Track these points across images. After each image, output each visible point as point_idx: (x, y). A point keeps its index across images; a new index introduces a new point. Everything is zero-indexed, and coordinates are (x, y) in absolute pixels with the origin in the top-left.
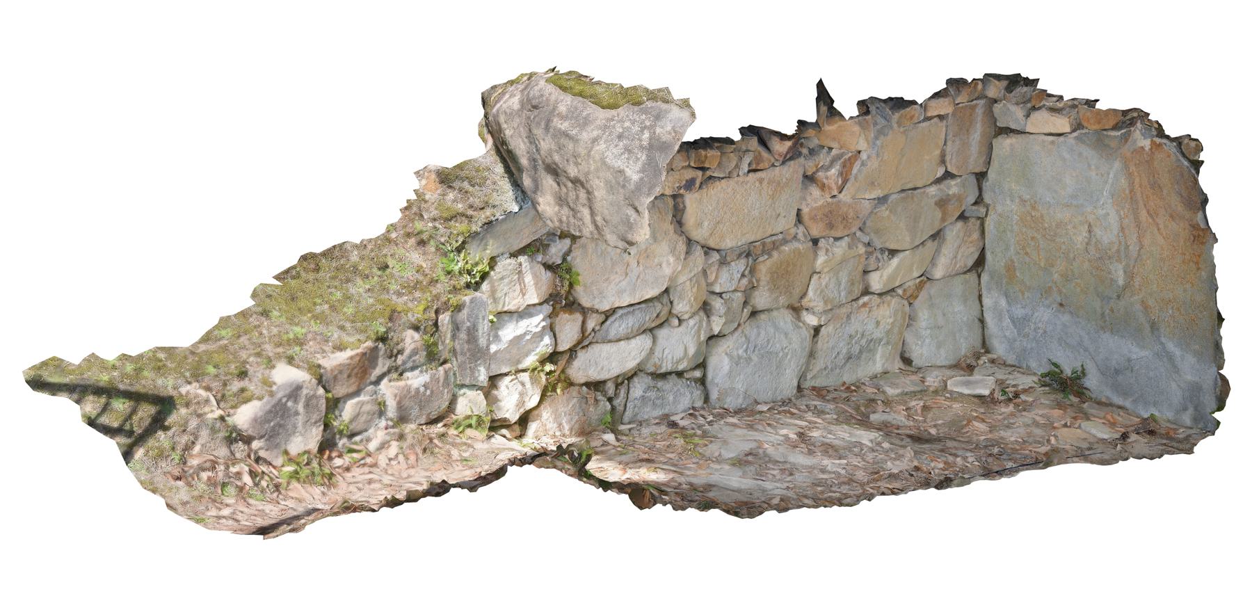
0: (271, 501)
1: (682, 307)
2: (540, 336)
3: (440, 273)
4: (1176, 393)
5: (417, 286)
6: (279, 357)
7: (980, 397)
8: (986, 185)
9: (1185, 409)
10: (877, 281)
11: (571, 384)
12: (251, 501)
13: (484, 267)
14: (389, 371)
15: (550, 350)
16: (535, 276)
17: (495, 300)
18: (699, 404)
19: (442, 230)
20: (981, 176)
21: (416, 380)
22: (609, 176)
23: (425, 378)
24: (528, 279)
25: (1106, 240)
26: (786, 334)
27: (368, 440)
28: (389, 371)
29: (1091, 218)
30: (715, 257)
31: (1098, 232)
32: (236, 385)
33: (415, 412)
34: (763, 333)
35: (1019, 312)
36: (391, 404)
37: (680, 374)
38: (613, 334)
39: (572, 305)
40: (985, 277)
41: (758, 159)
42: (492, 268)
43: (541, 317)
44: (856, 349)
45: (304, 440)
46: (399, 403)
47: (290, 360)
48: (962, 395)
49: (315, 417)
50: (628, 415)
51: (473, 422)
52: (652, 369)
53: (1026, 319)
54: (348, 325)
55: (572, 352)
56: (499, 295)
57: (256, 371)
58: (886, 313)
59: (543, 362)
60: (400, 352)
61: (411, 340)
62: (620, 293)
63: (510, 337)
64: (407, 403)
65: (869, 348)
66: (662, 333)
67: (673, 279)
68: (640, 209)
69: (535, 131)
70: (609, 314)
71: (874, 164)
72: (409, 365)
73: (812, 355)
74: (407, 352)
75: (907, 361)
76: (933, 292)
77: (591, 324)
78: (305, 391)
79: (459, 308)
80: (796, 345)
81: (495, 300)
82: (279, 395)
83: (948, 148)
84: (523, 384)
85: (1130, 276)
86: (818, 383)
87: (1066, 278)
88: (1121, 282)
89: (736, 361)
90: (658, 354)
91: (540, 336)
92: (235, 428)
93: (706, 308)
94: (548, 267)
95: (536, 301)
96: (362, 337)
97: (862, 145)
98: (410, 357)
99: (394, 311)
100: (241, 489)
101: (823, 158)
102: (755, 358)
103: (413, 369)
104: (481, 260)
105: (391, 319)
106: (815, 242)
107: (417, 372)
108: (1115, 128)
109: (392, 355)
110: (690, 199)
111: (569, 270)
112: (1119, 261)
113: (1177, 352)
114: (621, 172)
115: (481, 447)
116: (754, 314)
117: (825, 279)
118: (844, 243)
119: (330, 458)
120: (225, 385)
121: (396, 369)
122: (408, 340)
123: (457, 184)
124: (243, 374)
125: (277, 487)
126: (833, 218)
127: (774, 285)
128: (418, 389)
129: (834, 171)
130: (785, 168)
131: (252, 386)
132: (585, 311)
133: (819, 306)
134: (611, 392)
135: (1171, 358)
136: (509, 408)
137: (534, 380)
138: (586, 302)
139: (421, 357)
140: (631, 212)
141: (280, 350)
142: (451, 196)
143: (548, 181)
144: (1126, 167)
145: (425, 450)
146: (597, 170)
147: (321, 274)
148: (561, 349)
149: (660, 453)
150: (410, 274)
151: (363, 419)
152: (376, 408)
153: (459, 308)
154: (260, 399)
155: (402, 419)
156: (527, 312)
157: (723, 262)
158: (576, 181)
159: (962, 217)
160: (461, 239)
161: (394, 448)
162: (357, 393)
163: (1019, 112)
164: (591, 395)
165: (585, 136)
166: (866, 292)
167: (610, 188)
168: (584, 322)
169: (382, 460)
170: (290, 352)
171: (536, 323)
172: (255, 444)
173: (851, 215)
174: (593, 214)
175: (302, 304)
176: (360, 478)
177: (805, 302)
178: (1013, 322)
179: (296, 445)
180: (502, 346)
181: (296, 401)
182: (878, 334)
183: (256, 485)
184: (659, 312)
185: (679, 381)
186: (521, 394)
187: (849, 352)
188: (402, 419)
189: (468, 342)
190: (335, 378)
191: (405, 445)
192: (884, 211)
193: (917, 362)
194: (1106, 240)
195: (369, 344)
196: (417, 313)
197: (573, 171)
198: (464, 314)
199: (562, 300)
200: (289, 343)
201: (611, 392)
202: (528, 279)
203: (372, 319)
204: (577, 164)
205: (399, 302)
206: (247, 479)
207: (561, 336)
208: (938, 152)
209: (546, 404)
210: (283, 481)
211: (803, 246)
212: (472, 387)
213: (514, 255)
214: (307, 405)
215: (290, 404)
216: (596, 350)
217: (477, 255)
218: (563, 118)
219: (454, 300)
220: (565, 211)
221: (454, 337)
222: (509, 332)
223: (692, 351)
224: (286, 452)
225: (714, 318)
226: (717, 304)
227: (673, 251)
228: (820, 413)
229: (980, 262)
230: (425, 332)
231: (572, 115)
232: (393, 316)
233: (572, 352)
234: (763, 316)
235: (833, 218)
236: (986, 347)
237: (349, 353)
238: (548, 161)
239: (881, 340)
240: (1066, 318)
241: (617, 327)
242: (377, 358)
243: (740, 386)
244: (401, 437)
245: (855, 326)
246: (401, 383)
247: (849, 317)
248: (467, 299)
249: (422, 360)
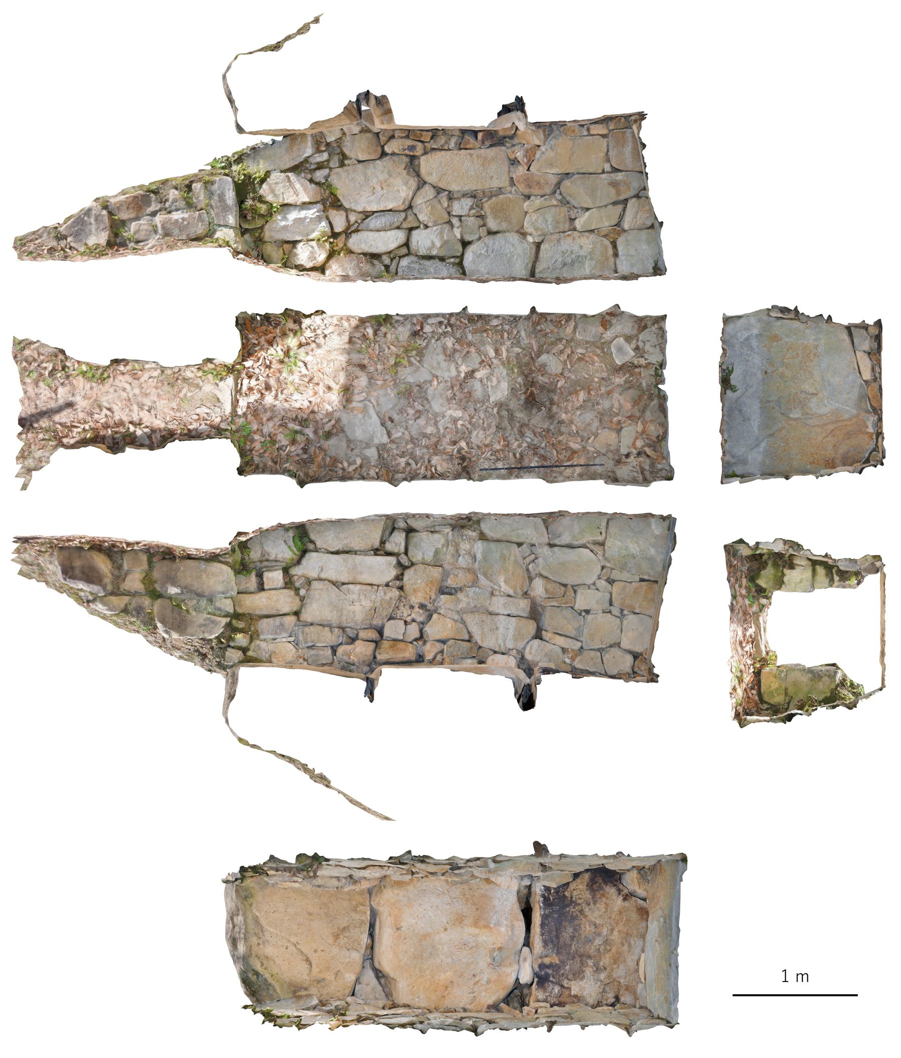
14: (160, 210)
16: (302, 185)
24: (298, 186)
25: (812, 405)
26: (513, 245)
28: (160, 210)
31: (814, 400)
34: (497, 243)
35: (754, 343)
38: (372, 226)
43: (315, 210)
44: (569, 260)
46: (162, 225)
49: (102, 226)
60: (167, 200)
62: (370, 202)
72: (173, 208)
74: (170, 200)
76: (629, 238)
78: (94, 212)
79: (213, 183)
83: (610, 153)
84: (312, 247)
85: (795, 419)
87: (782, 376)
88: (792, 416)
98: (172, 203)
103: (177, 210)
107: (180, 212)
113: (761, 449)
121: (166, 209)
122: (171, 194)
130: (489, 150)
132: (346, 210)
135: (757, 446)
152: (151, 228)
162: (137, 218)
168: (347, 216)
172: (69, 239)
173: (542, 181)
187: (563, 261)
189: (220, 201)
190: (118, 208)
198: (215, 187)
208: (602, 155)
212: (226, 226)
214: (96, 220)
224: (86, 244)
239: (586, 257)
240: (760, 376)
241: (373, 222)
247: (559, 241)
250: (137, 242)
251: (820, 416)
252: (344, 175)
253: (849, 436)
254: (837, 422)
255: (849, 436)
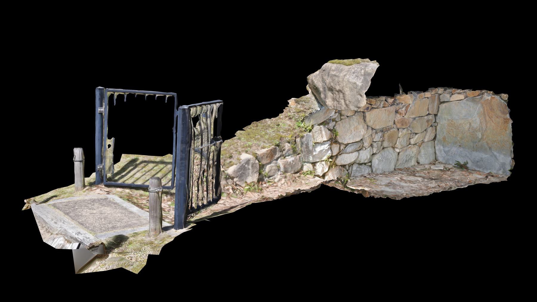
0: (239, 198)
1: (366, 144)
2: (327, 151)
3: (296, 126)
4: (497, 165)
5: (289, 130)
6: (243, 151)
7: (441, 170)
8: (437, 118)
9: (500, 170)
10: (412, 141)
11: (336, 165)
12: (232, 198)
13: (310, 127)
14: (281, 156)
15: (331, 155)
16: (325, 132)
17: (314, 139)
18: (370, 172)
19: (296, 115)
20: (436, 115)
21: (290, 159)
22: (351, 86)
23: (293, 159)
24: (324, 133)
25: (475, 126)
27: (275, 178)
28: (281, 156)
29: (471, 121)
30: (374, 131)
31: (473, 125)
32: (228, 161)
33: (290, 169)
35: (447, 149)
36: (282, 167)
37: (365, 164)
38: (348, 151)
39: (336, 142)
40: (436, 142)
41: (384, 104)
42: (313, 128)
44: (408, 159)
45: (252, 178)
46: (284, 166)
47: (247, 152)
48: (436, 170)
49: (255, 170)
50: (352, 175)
51: (309, 173)
52: (358, 162)
53: (449, 151)
54: (266, 141)
55: (337, 156)
56: (315, 137)
57: (235, 156)
58: (415, 149)
59: (329, 159)
60: (284, 150)
61: (287, 146)
62: (350, 139)
63: (319, 150)
64: (287, 166)
65: (410, 159)
66: (361, 152)
67: (363, 136)
68: (362, 95)
69: (324, 78)
70: (347, 145)
71: (413, 108)
72: (287, 154)
73: (398, 160)
74: (286, 150)
75: (418, 163)
77: (342, 148)
78: (251, 162)
79: (302, 137)
80: (394, 157)
81: (314, 139)
82: (242, 163)
83: (430, 106)
85: (483, 135)
86: (399, 167)
87: (462, 139)
88: (480, 137)
89: (380, 161)
90: (360, 158)
91: (327, 151)
92: (228, 174)
93: (372, 145)
94: (329, 130)
95: (326, 140)
96: (271, 144)
97: (411, 102)
99: (281, 137)
100: (229, 194)
101: (401, 106)
102: (384, 160)
103: (288, 156)
104: (309, 126)
105: (280, 139)
106: (398, 129)
107: (290, 157)
108: (478, 96)
109: (281, 151)
110: (367, 114)
111: (335, 131)
112: (480, 131)
113: (498, 155)
114: (355, 83)
115: (312, 180)
116: (383, 148)
117: (401, 139)
118: (406, 130)
119: (262, 184)
120: (225, 160)
121: (283, 155)
122: (286, 146)
123: (301, 103)
124: (231, 157)
125: (242, 193)
126: (403, 122)
127: (389, 141)
128: (290, 162)
129: (404, 109)
131: (234, 161)
132: (340, 144)
133: (400, 146)
134: (347, 168)
135: (495, 156)
136: (319, 172)
137: (326, 164)
138: (340, 141)
139: (291, 152)
140: (359, 97)
141: (243, 149)
142: (299, 106)
143: (329, 94)
144: (482, 105)
145: (293, 181)
146: (346, 85)
147: (258, 127)
148: (334, 155)
149: (363, 183)
150: (287, 127)
151: (273, 171)
152: (277, 168)
153: (302, 137)
154: (236, 164)
155: (286, 171)
156: (324, 143)
157: (376, 133)
158: (339, 91)
159: (431, 126)
160: (302, 118)
161: (283, 181)
162: (270, 163)
163: (448, 96)
164: (343, 169)
165: (342, 75)
166: (410, 144)
167: (351, 90)
169: (279, 184)
170: (247, 150)
171: (326, 146)
172: (235, 180)
174: (345, 101)
175: (252, 136)
176: (271, 190)
177: (396, 146)
178: (445, 152)
179: (249, 180)
180: (317, 153)
181: (248, 165)
182: (413, 155)
183: (234, 193)
184: (360, 146)
185: (366, 166)
186: (323, 168)
188: (286, 171)
189: (306, 148)
190: (262, 157)
191: (287, 179)
192: (415, 122)
193: (421, 163)
194: (475, 126)
195: (273, 147)
196: (289, 138)
197: (338, 88)
198: (304, 139)
199: (333, 140)
200: (247, 147)
201: (347, 168)
202: (324, 133)
203: (274, 139)
204: (339, 85)
205: (283, 135)
206: (231, 191)
207: (333, 151)
209: (330, 171)
210: (245, 192)
211: (396, 130)
212: (308, 162)
213: (319, 125)
214: (252, 166)
215: (246, 166)
216: (343, 155)
217: (308, 124)
218: (333, 71)
219: (301, 134)
220: (336, 102)
221: (301, 146)
222: (319, 149)
223: (369, 157)
224: (246, 182)
225: (374, 148)
226: (375, 144)
227: (364, 127)
228: (403, 174)
229: (435, 138)
230: (292, 144)
231: (337, 69)
232: (281, 138)
233: (337, 156)
234: (385, 149)
235: (403, 122)
236: (436, 159)
237: (266, 149)
238: (329, 86)
240: (461, 149)
241: (349, 149)
242: (276, 152)
243: (381, 168)
244: (285, 177)
245: (408, 153)
246: (285, 160)
248: (305, 134)
249: (292, 153)
250: (269, 177)
251: (481, 123)
252: (341, 124)
253: (492, 109)
254: (484, 114)
255: (492, 109)
